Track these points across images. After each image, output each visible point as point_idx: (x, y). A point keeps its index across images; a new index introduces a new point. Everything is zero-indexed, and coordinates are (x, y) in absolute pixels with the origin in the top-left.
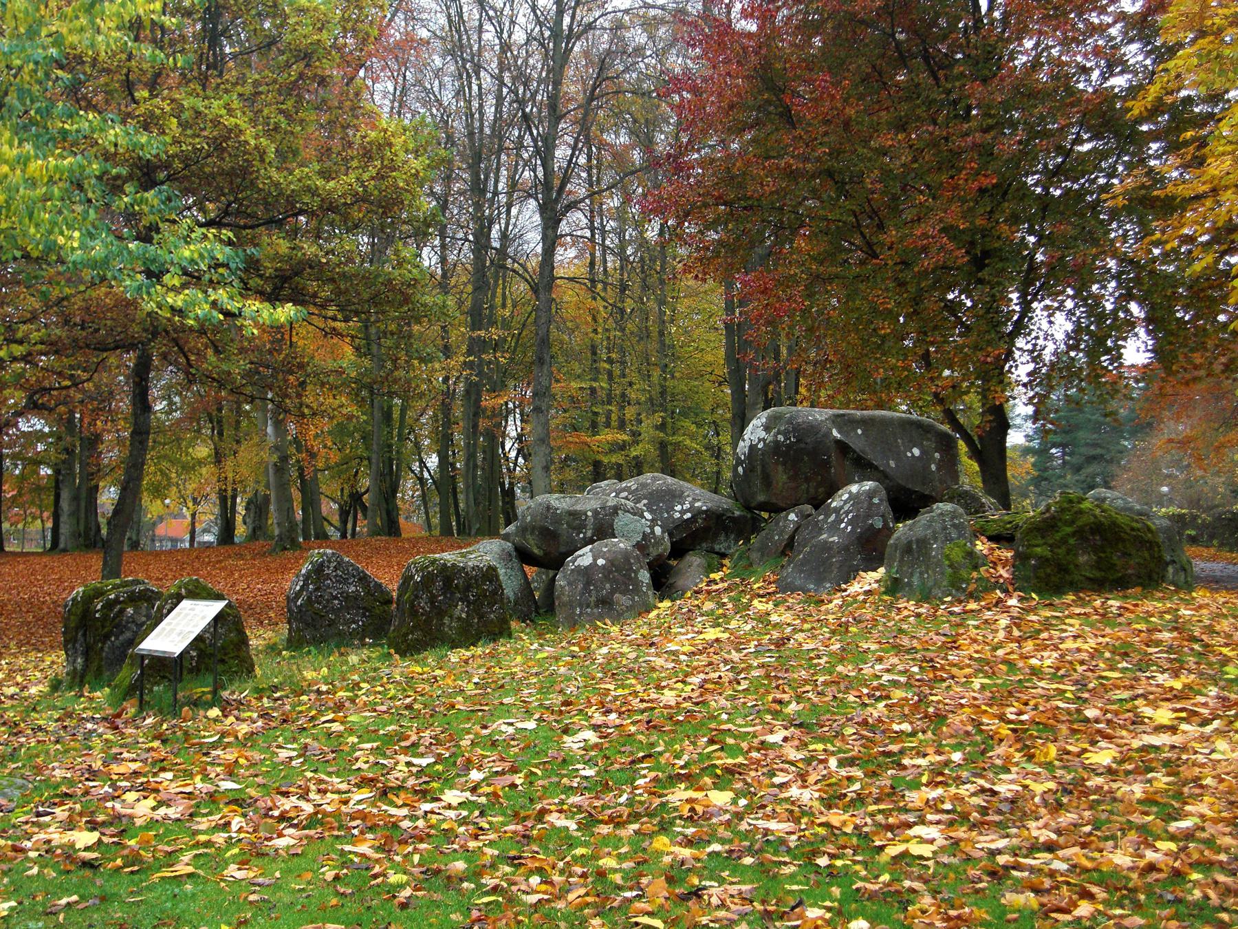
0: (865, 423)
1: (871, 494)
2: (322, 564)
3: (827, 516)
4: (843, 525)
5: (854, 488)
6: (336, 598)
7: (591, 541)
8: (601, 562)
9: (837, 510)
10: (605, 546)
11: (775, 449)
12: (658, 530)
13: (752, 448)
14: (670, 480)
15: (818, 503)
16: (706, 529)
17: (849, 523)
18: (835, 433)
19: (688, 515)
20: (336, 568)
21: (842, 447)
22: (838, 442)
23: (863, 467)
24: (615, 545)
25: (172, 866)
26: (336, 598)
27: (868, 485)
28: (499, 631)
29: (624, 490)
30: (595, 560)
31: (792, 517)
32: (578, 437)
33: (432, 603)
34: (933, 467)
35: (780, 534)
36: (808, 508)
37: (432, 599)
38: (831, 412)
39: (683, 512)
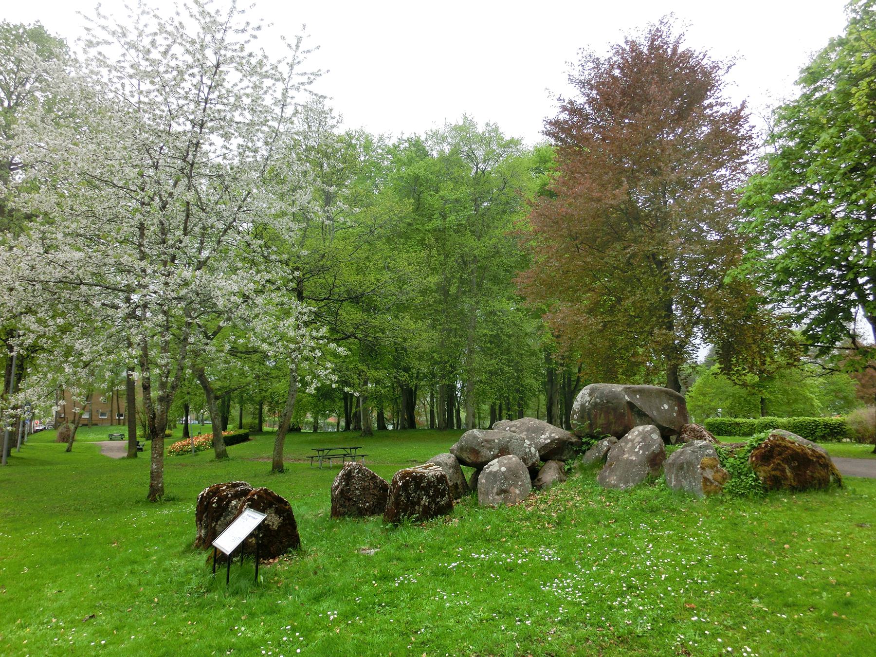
0: (641, 391)
1: (651, 432)
2: (350, 471)
3: (627, 443)
4: (637, 450)
5: (641, 428)
6: (357, 489)
7: (497, 456)
8: (503, 469)
9: (632, 441)
10: (505, 459)
11: (595, 405)
12: (533, 450)
13: (583, 406)
14: (537, 421)
15: (620, 436)
16: (558, 448)
17: (640, 448)
18: (627, 398)
19: (549, 441)
20: (358, 473)
21: (631, 405)
22: (628, 403)
23: (643, 417)
24: (511, 459)
25: (425, 462)
26: (357, 489)
27: (649, 427)
28: (446, 510)
29: (513, 426)
30: (500, 467)
31: (606, 443)
32: (317, 344)
33: (408, 498)
34: (675, 414)
35: (599, 453)
36: (614, 439)
37: (408, 496)
38: (623, 386)
39: (545, 439)
